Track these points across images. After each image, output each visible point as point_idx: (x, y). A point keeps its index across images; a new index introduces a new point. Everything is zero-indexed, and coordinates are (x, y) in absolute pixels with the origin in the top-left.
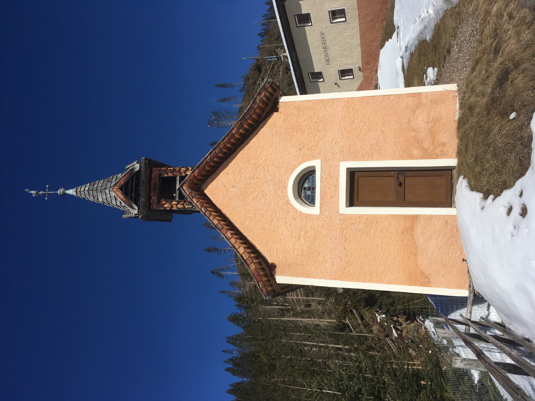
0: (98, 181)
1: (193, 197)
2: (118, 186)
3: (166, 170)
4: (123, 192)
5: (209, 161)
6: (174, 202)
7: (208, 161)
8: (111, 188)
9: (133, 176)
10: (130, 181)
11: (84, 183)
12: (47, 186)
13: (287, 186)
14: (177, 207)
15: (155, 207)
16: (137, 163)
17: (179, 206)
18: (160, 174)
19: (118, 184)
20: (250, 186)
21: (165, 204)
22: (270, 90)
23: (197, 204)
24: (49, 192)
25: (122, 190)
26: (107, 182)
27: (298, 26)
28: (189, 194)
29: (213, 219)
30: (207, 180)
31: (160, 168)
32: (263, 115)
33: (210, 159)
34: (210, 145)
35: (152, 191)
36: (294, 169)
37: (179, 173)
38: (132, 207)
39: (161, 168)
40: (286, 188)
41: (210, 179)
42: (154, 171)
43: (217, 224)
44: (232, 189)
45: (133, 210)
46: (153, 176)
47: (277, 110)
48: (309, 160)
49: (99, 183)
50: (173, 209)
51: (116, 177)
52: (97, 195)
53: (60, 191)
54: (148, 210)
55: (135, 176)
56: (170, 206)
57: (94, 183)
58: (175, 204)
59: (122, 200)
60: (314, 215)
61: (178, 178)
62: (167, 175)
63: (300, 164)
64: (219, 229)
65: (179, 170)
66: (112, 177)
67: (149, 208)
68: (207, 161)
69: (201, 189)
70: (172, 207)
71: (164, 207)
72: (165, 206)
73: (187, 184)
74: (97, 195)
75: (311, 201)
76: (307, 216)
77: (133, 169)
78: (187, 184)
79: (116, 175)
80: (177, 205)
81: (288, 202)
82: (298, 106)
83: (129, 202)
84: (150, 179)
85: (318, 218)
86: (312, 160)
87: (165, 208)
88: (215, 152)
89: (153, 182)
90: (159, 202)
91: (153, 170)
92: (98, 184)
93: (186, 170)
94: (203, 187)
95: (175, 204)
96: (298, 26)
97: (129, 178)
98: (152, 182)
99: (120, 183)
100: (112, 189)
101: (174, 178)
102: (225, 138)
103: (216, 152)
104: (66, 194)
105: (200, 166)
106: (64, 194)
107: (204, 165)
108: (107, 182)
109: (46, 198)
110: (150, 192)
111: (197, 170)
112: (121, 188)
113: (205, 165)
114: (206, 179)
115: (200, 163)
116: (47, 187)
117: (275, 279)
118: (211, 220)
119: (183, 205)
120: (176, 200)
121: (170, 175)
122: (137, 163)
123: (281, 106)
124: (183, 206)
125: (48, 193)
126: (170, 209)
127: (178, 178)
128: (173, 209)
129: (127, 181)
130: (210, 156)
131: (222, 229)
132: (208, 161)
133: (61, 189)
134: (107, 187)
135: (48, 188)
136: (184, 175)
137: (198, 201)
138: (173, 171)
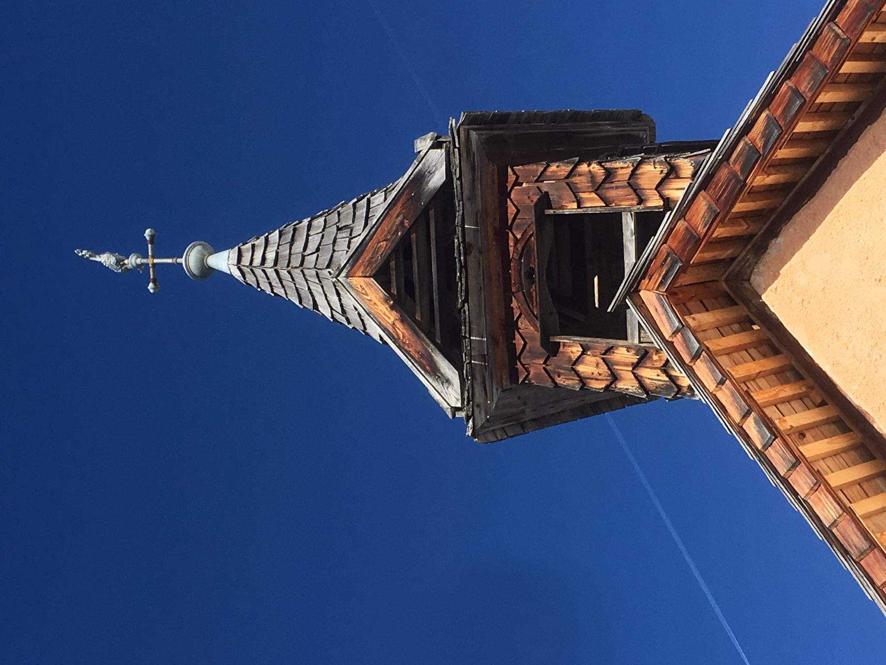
0: (306, 222)
1: (696, 357)
2: (370, 263)
3: (570, 174)
4: (394, 291)
5: (765, 146)
7: (760, 144)
8: (343, 274)
9: (425, 212)
10: (414, 236)
11: (262, 228)
12: (148, 232)
14: (637, 377)
15: (535, 367)
16: (433, 147)
18: (545, 201)
19: (366, 256)
23: (719, 395)
24: (156, 261)
25: (385, 285)
26: (339, 229)
27: (642, 341)
28: (675, 333)
29: (813, 490)
30: (776, 236)
31: (541, 169)
33: (766, 135)
35: (514, 290)
37: (635, 191)
38: (434, 371)
39: (548, 166)
41: (789, 231)
42: (517, 183)
43: (834, 523)
45: (439, 387)
46: (512, 210)
49: (311, 233)
50: (621, 385)
51: (365, 210)
52: (309, 289)
53: (191, 259)
54: (506, 383)
56: (604, 369)
57: (295, 230)
58: (626, 365)
59: (389, 335)
61: (629, 224)
62: (575, 205)
64: (846, 553)
65: (633, 174)
66: (354, 204)
67: (514, 374)
68: (753, 149)
69: (746, 285)
70: (615, 377)
71: (577, 373)
72: (581, 368)
73: (657, 278)
74: (309, 289)
78: (657, 278)
79: (365, 200)
80: (636, 366)
83: (419, 348)
84: (503, 228)
87: (582, 380)
88: (796, 92)
89: (517, 241)
90: (553, 350)
91: (512, 178)
92: (308, 236)
93: (668, 174)
94: (756, 280)
95: (626, 365)
96: (642, 341)
97: (407, 223)
98: (511, 243)
99: (376, 252)
100: (347, 276)
101: (615, 219)
103: (802, 89)
104: (211, 269)
105: (717, 176)
106: (207, 272)
107: (737, 168)
108: (339, 229)
109: (151, 285)
111: (700, 198)
112: (382, 276)
113: (742, 170)
114: (773, 232)
115: (716, 159)
116: (148, 238)
118: (802, 495)
120: (630, 341)
121: (593, 203)
122: (437, 145)
124: (664, 378)
125: (154, 265)
126: (607, 388)
127: (629, 224)
128: (621, 385)
129: (402, 237)
130: (764, 115)
131: (863, 553)
132: (760, 144)
133: (194, 246)
134: (335, 254)
135: (152, 242)
136: (655, 202)
137: (722, 382)
138: (604, 181)
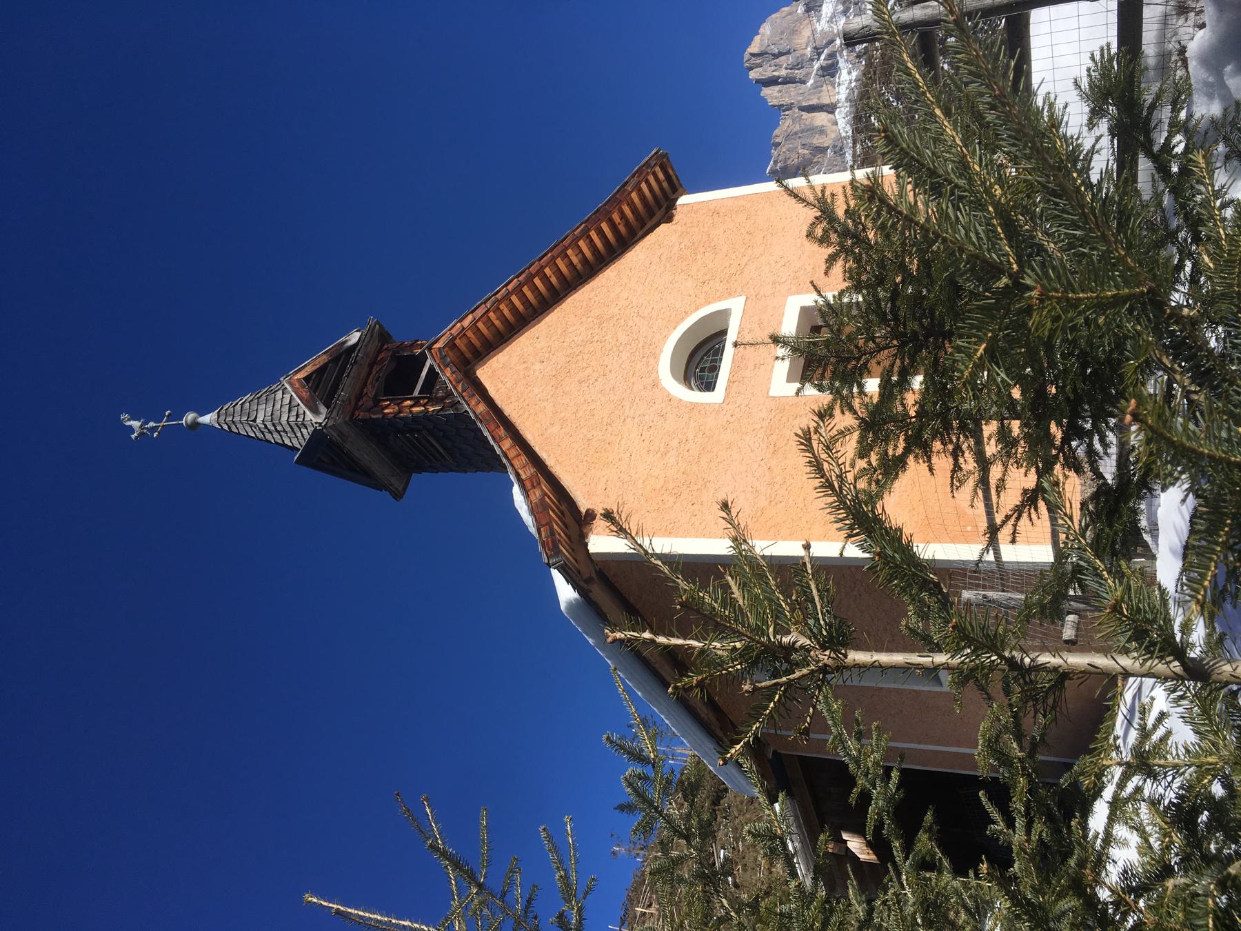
6: (409, 402)
9: (342, 353)
13: (661, 351)
17: (416, 409)
20: (580, 358)
21: (387, 407)
22: (661, 176)
32: (640, 233)
34: (615, 809)
36: (683, 319)
38: (315, 411)
40: (656, 357)
44: (538, 366)
47: (669, 218)
48: (720, 299)
55: (344, 356)
60: (709, 404)
63: (697, 309)
72: (386, 411)
75: (709, 386)
76: (694, 406)
77: (345, 342)
81: (656, 384)
82: (714, 211)
85: (718, 409)
86: (726, 298)
90: (377, 401)
102: (546, 255)
106: (195, 425)
110: (365, 385)
117: (586, 545)
119: (424, 406)
123: (679, 215)
